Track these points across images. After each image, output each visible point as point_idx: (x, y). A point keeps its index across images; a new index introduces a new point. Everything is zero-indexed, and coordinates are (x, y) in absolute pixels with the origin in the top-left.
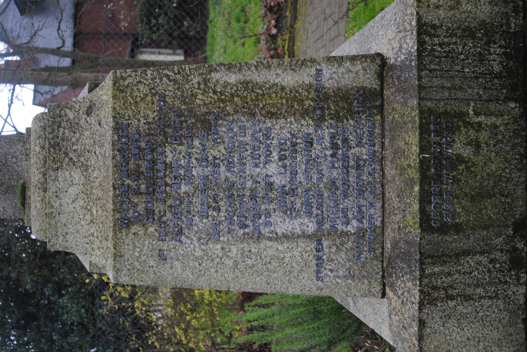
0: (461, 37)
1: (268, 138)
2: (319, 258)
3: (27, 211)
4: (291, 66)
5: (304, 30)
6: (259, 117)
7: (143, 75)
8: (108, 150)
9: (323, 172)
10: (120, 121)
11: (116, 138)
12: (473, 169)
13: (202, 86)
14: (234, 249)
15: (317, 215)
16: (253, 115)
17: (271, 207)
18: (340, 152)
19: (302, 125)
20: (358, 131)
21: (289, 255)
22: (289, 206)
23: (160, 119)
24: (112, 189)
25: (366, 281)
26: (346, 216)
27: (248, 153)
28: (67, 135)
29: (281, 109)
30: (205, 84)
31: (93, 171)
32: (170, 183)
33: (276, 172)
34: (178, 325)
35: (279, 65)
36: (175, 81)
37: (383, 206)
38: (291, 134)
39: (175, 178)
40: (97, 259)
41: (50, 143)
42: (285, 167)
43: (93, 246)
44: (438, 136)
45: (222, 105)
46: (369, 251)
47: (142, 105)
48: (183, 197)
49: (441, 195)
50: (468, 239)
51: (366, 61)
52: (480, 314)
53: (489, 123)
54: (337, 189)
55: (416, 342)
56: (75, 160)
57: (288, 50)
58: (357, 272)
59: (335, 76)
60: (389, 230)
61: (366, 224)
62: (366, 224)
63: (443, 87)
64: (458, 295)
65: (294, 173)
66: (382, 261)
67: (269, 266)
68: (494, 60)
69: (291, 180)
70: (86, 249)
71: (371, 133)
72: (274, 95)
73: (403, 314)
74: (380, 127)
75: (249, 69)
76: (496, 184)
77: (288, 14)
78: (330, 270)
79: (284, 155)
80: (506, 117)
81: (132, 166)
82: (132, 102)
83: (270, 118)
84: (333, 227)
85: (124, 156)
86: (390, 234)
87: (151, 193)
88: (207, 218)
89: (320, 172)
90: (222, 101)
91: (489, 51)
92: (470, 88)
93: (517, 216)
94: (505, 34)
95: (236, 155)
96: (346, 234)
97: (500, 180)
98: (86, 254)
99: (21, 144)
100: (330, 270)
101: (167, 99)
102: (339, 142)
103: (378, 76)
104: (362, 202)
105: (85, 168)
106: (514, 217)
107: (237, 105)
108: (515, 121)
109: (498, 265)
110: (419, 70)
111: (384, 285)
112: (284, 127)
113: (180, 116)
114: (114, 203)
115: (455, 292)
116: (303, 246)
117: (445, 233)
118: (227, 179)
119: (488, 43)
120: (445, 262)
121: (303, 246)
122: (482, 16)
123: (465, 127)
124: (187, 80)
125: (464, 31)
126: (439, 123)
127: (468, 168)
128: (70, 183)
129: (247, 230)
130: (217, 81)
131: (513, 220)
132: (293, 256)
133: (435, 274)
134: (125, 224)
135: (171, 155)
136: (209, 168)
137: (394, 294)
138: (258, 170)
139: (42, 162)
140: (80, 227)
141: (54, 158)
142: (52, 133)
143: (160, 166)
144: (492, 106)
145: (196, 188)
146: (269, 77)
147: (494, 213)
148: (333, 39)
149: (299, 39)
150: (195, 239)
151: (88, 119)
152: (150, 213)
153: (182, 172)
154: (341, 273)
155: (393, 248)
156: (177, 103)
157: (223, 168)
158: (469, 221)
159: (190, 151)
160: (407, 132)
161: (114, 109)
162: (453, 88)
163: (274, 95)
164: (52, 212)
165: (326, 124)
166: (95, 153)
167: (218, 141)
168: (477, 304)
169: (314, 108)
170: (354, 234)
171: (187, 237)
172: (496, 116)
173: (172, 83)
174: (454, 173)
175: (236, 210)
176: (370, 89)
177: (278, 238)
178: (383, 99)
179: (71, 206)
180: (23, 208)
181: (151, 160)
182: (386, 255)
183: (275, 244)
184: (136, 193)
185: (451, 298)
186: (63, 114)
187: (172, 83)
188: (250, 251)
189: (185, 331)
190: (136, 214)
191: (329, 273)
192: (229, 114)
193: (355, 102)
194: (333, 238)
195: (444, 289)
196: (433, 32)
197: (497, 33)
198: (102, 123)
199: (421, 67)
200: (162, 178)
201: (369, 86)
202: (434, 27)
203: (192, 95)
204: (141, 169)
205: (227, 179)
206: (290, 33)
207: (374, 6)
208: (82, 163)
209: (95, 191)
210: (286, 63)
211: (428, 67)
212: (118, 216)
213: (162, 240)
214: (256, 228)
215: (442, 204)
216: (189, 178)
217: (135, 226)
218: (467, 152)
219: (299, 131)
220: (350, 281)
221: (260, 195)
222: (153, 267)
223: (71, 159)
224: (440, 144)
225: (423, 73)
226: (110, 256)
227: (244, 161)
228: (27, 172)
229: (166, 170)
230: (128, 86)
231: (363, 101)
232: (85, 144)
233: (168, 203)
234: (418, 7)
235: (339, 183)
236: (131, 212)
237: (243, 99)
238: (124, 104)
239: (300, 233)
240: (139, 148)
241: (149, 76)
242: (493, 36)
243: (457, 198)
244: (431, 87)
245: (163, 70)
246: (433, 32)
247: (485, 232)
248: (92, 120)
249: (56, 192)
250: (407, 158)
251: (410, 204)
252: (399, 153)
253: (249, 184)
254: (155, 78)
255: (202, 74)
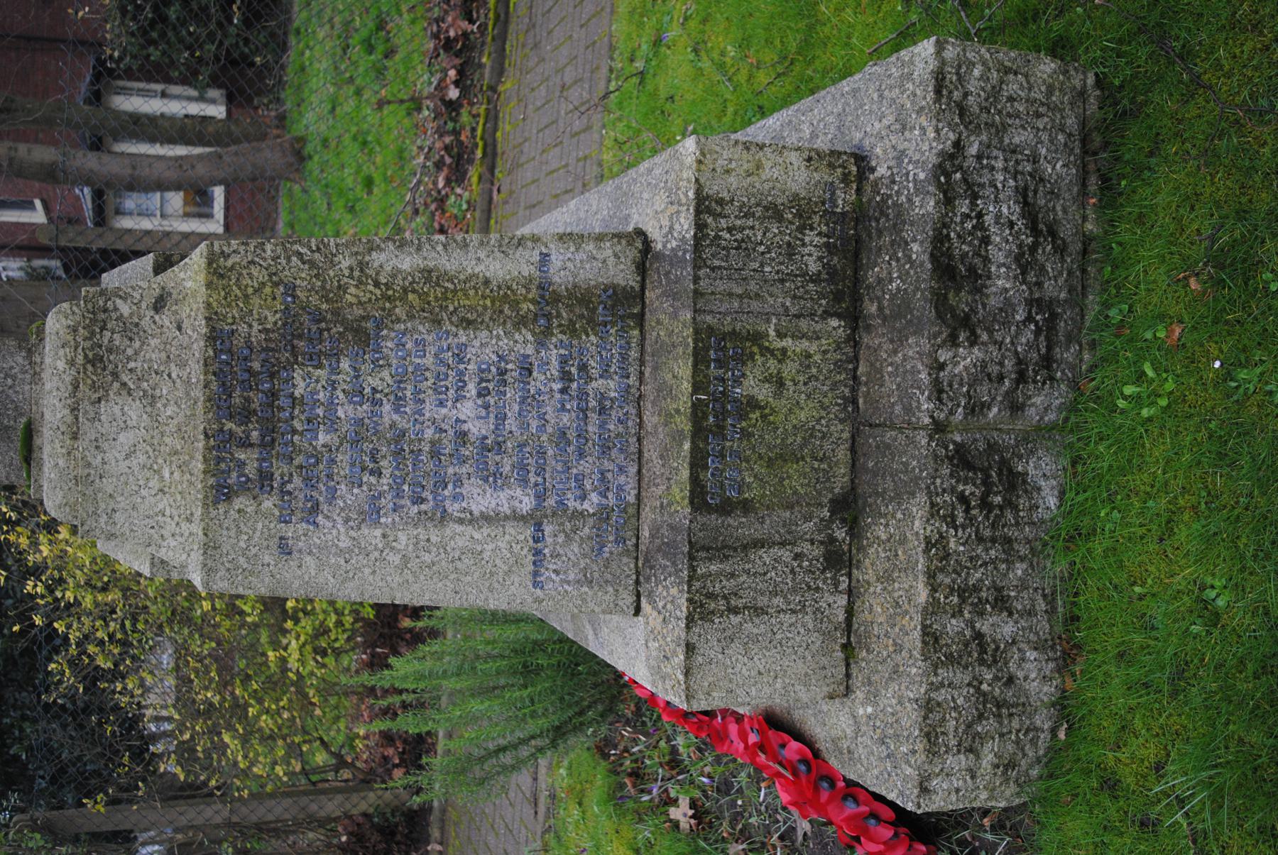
0: (762, 219)
1: (461, 361)
2: (537, 553)
3: (34, 472)
4: (500, 246)
5: (520, 100)
6: (447, 326)
7: (258, 251)
8: (195, 371)
9: (547, 417)
10: (218, 326)
11: (211, 353)
12: (771, 418)
13: (356, 274)
14: (402, 537)
15: (536, 485)
16: (438, 322)
17: (464, 470)
18: (574, 386)
19: (516, 342)
20: (604, 353)
21: (491, 546)
22: (492, 469)
23: (284, 325)
24: (202, 437)
25: (610, 589)
26: (581, 486)
27: (429, 383)
28: (117, 343)
29: (482, 314)
30: (362, 271)
31: (165, 406)
32: (300, 429)
33: (472, 415)
34: (230, 728)
35: (482, 243)
36: (312, 264)
37: (639, 472)
38: (498, 356)
39: (309, 421)
40: (171, 553)
41: (86, 356)
42: (486, 407)
43: (163, 532)
44: (721, 368)
45: (387, 305)
46: (617, 541)
47: (256, 301)
48: (321, 453)
49: (723, 456)
50: (762, 523)
51: (619, 243)
52: (778, 636)
53: (798, 350)
54: (569, 443)
55: (681, 677)
56: (132, 386)
57: (482, 138)
58: (596, 575)
59: (569, 264)
60: (647, 509)
61: (612, 500)
62: (612, 500)
63: (731, 295)
64: (744, 608)
65: (501, 418)
66: (637, 558)
67: (459, 564)
68: (810, 255)
69: (497, 428)
70: (151, 536)
71: (624, 358)
72: (472, 292)
73: (664, 637)
74: (638, 348)
75: (433, 248)
76: (805, 442)
77: (484, 60)
78: (555, 571)
79: (487, 388)
80: (824, 342)
81: (237, 400)
82: (239, 294)
83: (465, 329)
84: (560, 503)
85: (224, 384)
86: (648, 515)
87: (267, 444)
88: (360, 486)
89: (542, 417)
90: (389, 299)
91: (802, 240)
92: (771, 295)
93: (836, 491)
94: (829, 215)
95: (409, 387)
96: (582, 514)
97: (811, 436)
98: (149, 545)
99: (24, 354)
100: (555, 571)
101: (299, 293)
102: (574, 370)
103: (637, 268)
104: (607, 465)
105: (151, 399)
106: (832, 492)
107: (412, 307)
108: (838, 348)
109: (806, 564)
110: (696, 267)
111: (638, 596)
112: (487, 343)
113: (319, 321)
114: (205, 460)
115: (740, 603)
116: (513, 532)
117: (728, 514)
118: (393, 425)
119: (801, 229)
120: (726, 557)
121: (513, 532)
122: (794, 188)
123: (762, 355)
124: (332, 261)
125: (766, 209)
126: (724, 349)
127: (764, 417)
128: (123, 425)
129: (423, 507)
130: (381, 266)
131: (830, 496)
132: (498, 548)
133: (710, 575)
134: (224, 494)
135: (302, 384)
136: (365, 407)
137: (654, 608)
138: (444, 411)
139: (70, 387)
140: (139, 500)
141: (94, 382)
142: (90, 339)
143: (283, 401)
144: (804, 324)
145: (343, 439)
146: (465, 263)
147: (802, 485)
148: (576, 134)
149: (507, 117)
150: (339, 520)
151: (157, 318)
152: (265, 477)
153: (320, 411)
154: (572, 577)
155: (652, 536)
156: (314, 300)
157: (387, 407)
158: (764, 496)
159: (333, 377)
160: (676, 359)
161: (209, 305)
162: (746, 295)
163: (472, 292)
164: (89, 475)
165: (554, 340)
166: (169, 376)
167: (381, 362)
168: (773, 620)
169: (536, 315)
170: (594, 514)
171: (327, 517)
172: (810, 339)
173: (307, 266)
174: (744, 424)
175: (407, 475)
176: (624, 288)
177: (473, 520)
178: (644, 303)
179: (123, 465)
180: (25, 465)
181: (269, 391)
182: (642, 547)
183: (469, 530)
184: (243, 445)
185: (735, 611)
186: (111, 308)
187: (307, 266)
188: (428, 540)
189: (245, 740)
190: (243, 479)
191: (553, 576)
192: (398, 320)
193: (601, 307)
194: (560, 521)
195: (725, 597)
196: (719, 209)
197: (815, 213)
198: (184, 326)
199: (698, 263)
200: (286, 421)
201: (623, 283)
202: (721, 202)
203: (339, 287)
204: (253, 406)
205: (393, 425)
206: (489, 102)
207: (656, 89)
208: (145, 391)
209: (167, 440)
210: (492, 242)
211: (709, 263)
212: (212, 481)
213: (286, 522)
214: (439, 504)
215: (723, 471)
216: (332, 422)
217: (241, 499)
218: (763, 393)
219: (511, 350)
220: (585, 589)
221: (447, 451)
222: (268, 565)
223: (124, 384)
224: (723, 380)
225: (701, 273)
226: (196, 547)
227: (422, 396)
228: (36, 404)
229: (293, 408)
230: (232, 268)
231: (613, 306)
232: (151, 360)
233: (296, 462)
234: (699, 170)
235: (572, 435)
236: (234, 475)
237: (422, 296)
238: (225, 298)
239: (508, 512)
240: (249, 370)
241: (269, 252)
242: (810, 218)
243: (748, 461)
244: (713, 293)
245: (291, 244)
246: (719, 209)
247: (788, 514)
248: (165, 319)
249: (96, 440)
250: (675, 399)
251: (677, 469)
252: (665, 391)
253: (429, 433)
254: (279, 257)
255: (357, 253)
